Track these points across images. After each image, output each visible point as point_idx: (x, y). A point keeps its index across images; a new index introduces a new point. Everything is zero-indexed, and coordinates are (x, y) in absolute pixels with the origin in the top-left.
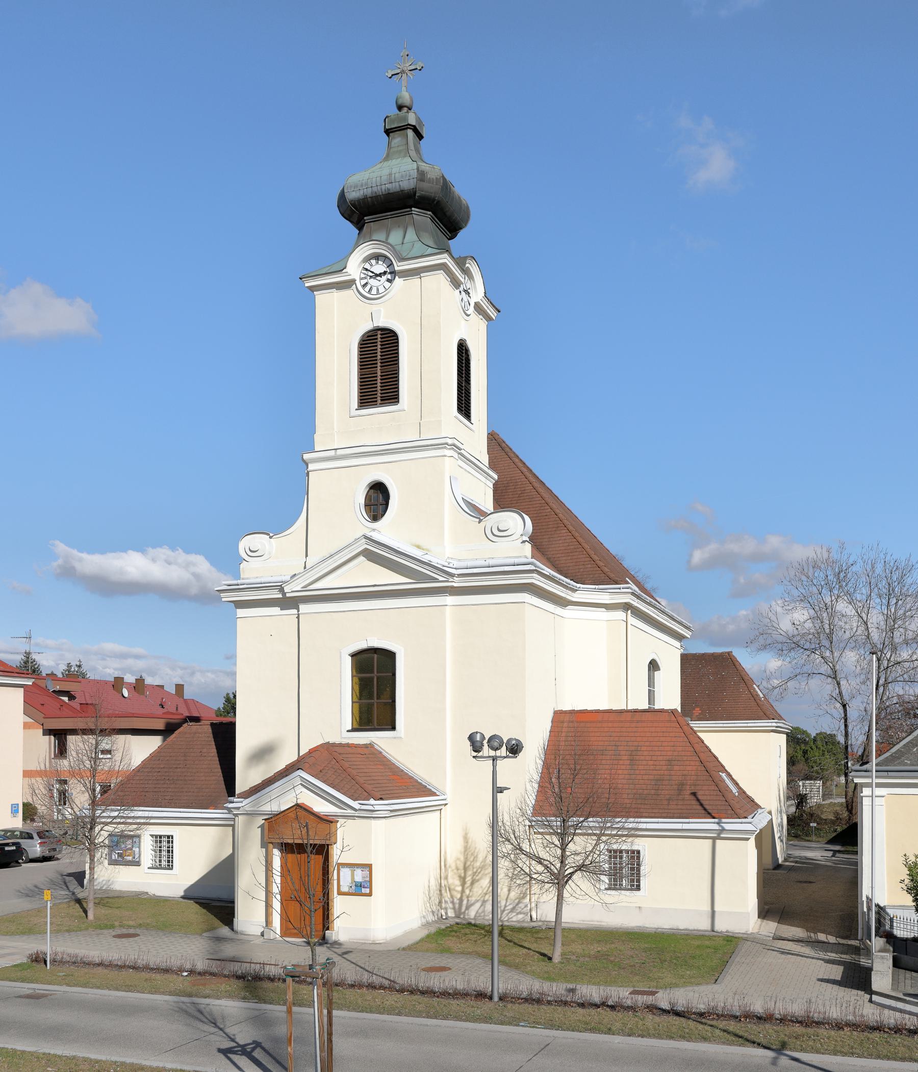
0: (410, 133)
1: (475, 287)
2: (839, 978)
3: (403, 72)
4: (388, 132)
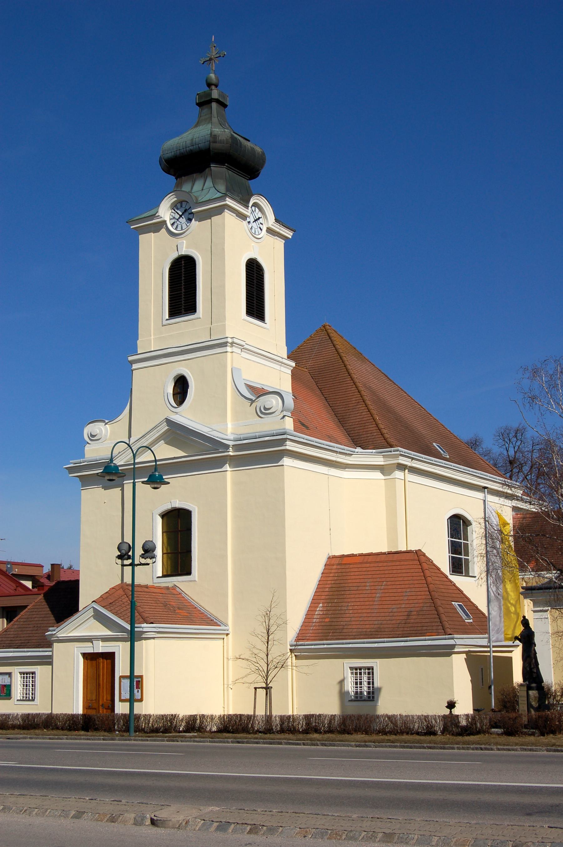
0: (214, 105)
1: (266, 217)
2: (125, 581)
3: (211, 59)
4: (200, 105)
